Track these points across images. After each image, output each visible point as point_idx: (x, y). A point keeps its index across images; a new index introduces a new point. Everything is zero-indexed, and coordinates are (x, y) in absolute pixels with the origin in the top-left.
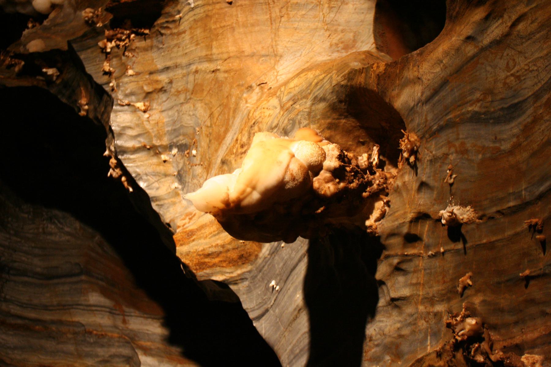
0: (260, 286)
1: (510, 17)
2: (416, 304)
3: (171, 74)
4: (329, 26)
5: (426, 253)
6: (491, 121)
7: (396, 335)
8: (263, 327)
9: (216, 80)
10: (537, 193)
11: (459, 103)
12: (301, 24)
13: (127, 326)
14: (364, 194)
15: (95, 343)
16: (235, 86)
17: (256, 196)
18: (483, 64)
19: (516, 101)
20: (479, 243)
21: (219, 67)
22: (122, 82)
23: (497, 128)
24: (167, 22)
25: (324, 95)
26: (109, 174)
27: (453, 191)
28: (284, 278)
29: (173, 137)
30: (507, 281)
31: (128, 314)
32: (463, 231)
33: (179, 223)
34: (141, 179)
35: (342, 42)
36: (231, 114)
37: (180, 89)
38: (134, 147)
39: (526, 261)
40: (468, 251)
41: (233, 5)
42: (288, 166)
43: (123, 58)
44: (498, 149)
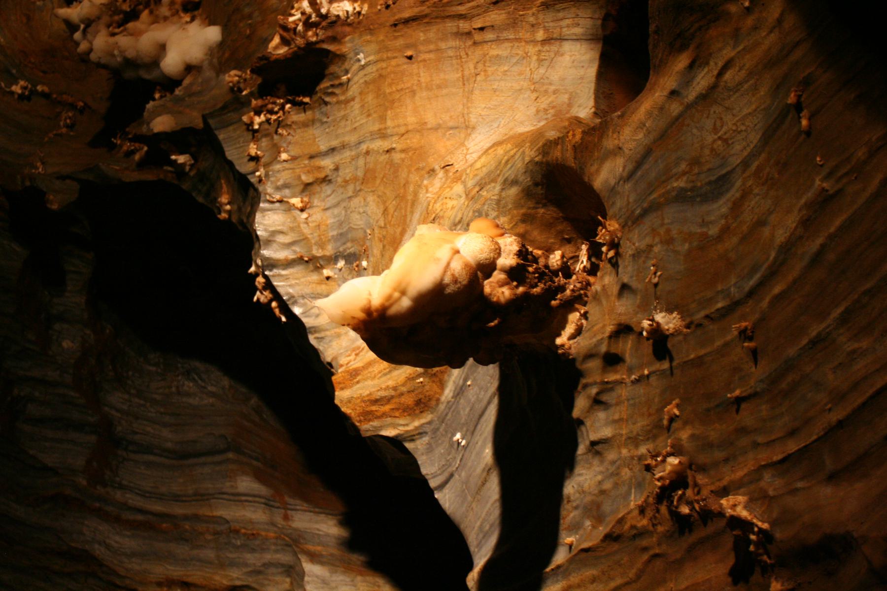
0: (442, 443)
1: (716, 64)
2: (619, 447)
3: (337, 158)
4: (537, 86)
5: (629, 377)
6: (698, 199)
7: (596, 492)
8: (446, 499)
9: (391, 163)
10: (747, 289)
11: (663, 178)
12: (502, 83)
13: (290, 523)
14: (553, 303)
15: (243, 546)
16: (413, 170)
17: (406, 303)
18: (688, 125)
19: (724, 172)
20: (686, 359)
21: (394, 146)
22: (273, 171)
23: (705, 208)
24: (332, 86)
25: (516, 176)
26: (255, 299)
27: (658, 293)
28: (472, 428)
29: (339, 244)
30: (718, 406)
31: (292, 507)
32: (669, 345)
33: (343, 360)
34: (295, 303)
35: (553, 107)
36: (409, 209)
37: (348, 178)
38: (286, 260)
39: (736, 378)
40: (675, 371)
41: (413, 60)
42: (448, 264)
43: (276, 137)
44: (705, 235)
